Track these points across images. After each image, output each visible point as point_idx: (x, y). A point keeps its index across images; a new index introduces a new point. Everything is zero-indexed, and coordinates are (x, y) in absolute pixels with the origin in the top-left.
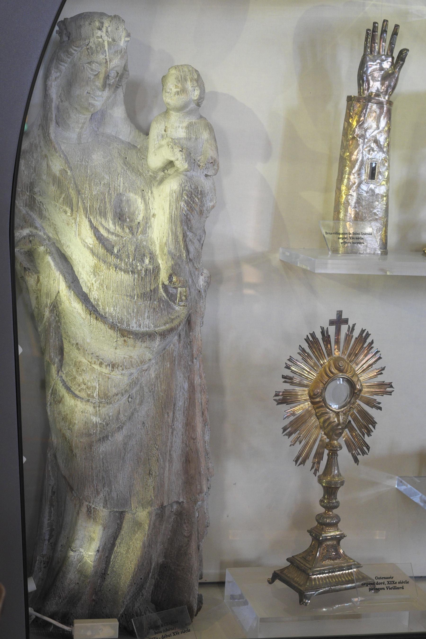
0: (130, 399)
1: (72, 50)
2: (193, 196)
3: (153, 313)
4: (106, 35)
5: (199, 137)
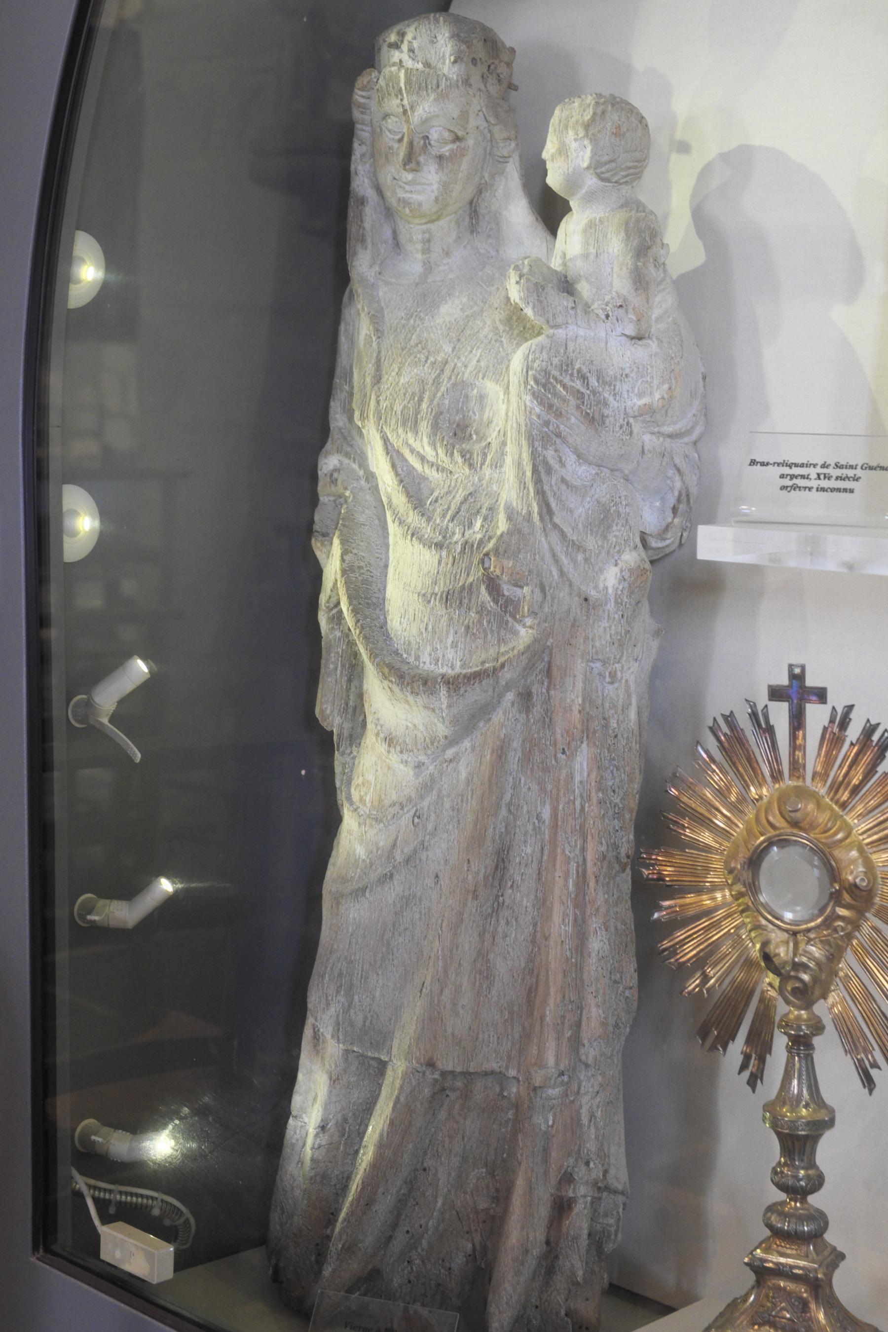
0: (416, 820)
1: (357, 97)
2: (552, 380)
3: (466, 636)
4: (410, 57)
5: (602, 250)
